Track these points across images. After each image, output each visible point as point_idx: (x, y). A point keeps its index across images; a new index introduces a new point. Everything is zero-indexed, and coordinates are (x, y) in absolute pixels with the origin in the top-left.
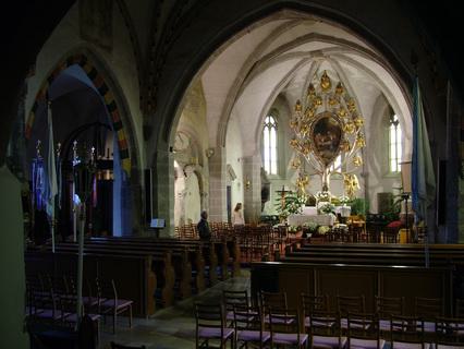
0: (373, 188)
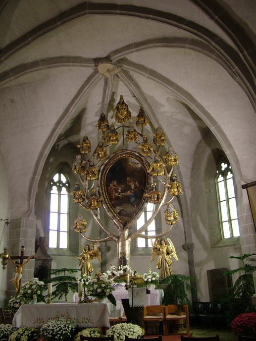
0: (200, 264)
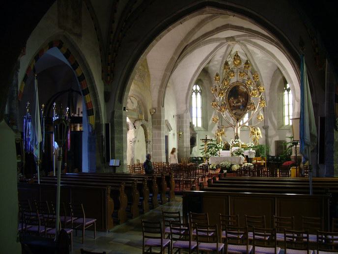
0: (272, 137)
